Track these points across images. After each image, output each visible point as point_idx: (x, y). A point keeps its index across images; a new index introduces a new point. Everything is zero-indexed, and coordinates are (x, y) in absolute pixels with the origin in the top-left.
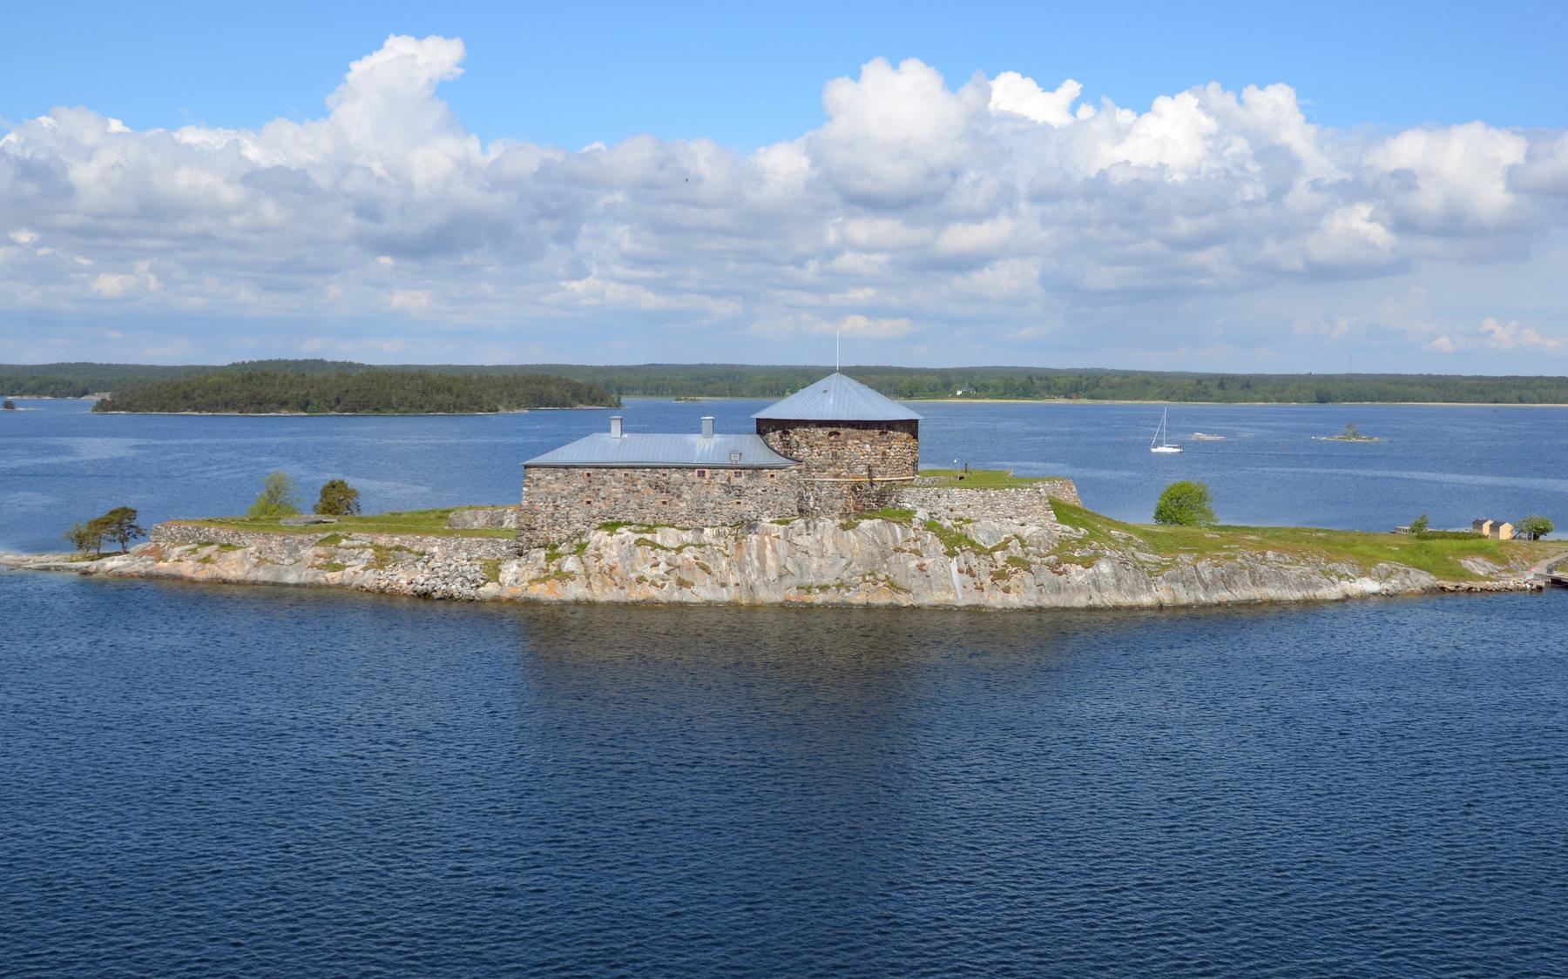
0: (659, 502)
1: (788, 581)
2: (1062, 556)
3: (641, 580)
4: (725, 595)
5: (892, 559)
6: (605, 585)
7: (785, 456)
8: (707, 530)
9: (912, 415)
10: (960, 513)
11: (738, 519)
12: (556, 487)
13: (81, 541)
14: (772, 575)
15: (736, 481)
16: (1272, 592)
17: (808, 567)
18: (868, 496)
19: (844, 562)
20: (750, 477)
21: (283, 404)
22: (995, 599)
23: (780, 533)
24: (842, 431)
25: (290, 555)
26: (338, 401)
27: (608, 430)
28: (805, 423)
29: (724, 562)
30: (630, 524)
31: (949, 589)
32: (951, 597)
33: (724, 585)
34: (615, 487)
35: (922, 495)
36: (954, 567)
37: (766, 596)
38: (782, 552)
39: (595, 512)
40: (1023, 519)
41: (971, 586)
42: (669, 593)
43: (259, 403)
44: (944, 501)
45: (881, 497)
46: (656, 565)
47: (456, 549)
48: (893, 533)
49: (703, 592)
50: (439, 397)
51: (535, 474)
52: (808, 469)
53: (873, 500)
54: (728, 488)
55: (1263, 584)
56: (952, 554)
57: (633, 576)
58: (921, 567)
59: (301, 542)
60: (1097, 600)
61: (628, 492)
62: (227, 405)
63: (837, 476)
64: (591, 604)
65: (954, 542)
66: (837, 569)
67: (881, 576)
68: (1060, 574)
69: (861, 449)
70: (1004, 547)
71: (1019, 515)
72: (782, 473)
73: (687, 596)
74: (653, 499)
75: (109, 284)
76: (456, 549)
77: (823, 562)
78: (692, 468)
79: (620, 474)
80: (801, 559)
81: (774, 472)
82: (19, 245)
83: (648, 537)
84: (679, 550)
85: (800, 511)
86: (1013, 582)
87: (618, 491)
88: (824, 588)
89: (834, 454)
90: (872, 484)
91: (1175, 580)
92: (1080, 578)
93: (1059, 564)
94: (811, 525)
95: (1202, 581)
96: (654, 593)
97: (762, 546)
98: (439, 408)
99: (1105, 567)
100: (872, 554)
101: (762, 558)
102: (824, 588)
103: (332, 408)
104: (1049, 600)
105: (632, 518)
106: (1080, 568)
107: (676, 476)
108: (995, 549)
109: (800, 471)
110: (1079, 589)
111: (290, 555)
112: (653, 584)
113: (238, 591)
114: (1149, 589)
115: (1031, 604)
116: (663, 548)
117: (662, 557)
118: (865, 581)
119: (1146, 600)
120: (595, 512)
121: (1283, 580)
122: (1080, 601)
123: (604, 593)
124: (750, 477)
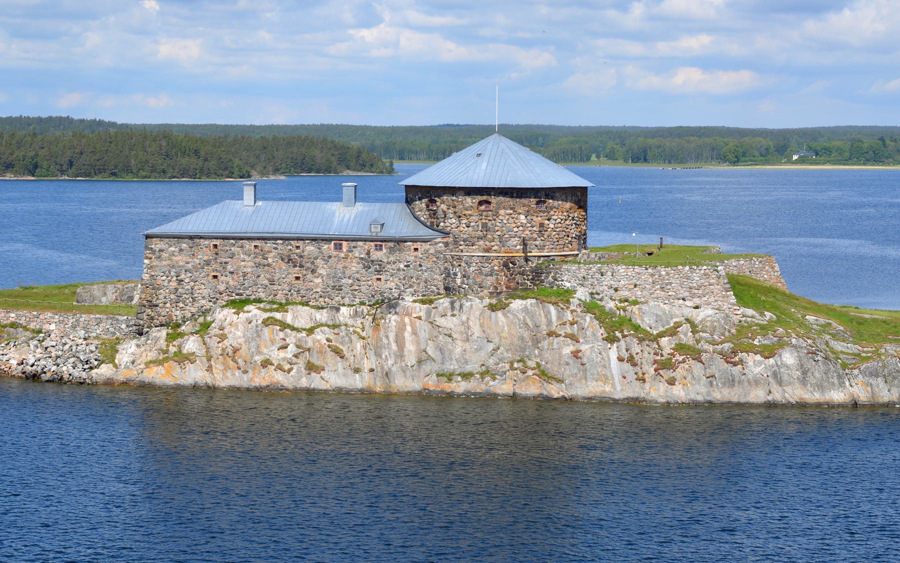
0: (291, 278)
1: (427, 367)
3: (266, 363)
4: (358, 382)
5: (545, 344)
6: (227, 368)
7: (431, 227)
10: (624, 293)
11: (378, 297)
12: (180, 259)
14: (411, 360)
15: (376, 255)
17: (451, 352)
19: (491, 347)
20: (391, 251)
22: (657, 392)
23: (422, 314)
24: (494, 200)
26: (71, 164)
28: (452, 191)
29: (359, 345)
30: (259, 301)
31: (606, 379)
32: (608, 388)
33: (357, 371)
34: (243, 260)
35: (583, 272)
36: (613, 354)
37: (403, 383)
38: (423, 335)
41: (631, 376)
44: (607, 280)
45: (537, 273)
47: (74, 327)
48: (548, 314)
49: (334, 377)
50: (184, 161)
51: (157, 245)
52: (456, 242)
53: (527, 278)
54: (368, 263)
57: (258, 359)
58: (576, 354)
61: (258, 265)
63: (488, 250)
64: (211, 389)
65: (615, 326)
66: (483, 353)
67: (531, 364)
69: (515, 221)
70: (672, 332)
71: (693, 296)
72: (426, 246)
73: (316, 382)
74: (285, 273)
76: (74, 327)
77: (467, 346)
78: (328, 240)
79: (249, 246)
80: (448, 342)
81: (416, 245)
83: (278, 316)
84: (310, 331)
86: (679, 372)
87: (248, 265)
88: (466, 376)
89: (485, 226)
90: (527, 259)
91: (875, 374)
92: (757, 370)
93: (734, 353)
94: (457, 305)
96: (280, 378)
97: (401, 328)
99: (788, 358)
100: (522, 338)
102: (466, 376)
103: (63, 172)
104: (720, 394)
105: (262, 295)
106: (758, 357)
107: (310, 248)
109: (446, 244)
110: (757, 382)
112: (280, 368)
114: (842, 384)
115: (700, 398)
116: (293, 329)
117: (292, 338)
118: (512, 368)
119: (837, 396)
120: (222, 287)
122: (758, 395)
123: (225, 377)
124: (391, 251)
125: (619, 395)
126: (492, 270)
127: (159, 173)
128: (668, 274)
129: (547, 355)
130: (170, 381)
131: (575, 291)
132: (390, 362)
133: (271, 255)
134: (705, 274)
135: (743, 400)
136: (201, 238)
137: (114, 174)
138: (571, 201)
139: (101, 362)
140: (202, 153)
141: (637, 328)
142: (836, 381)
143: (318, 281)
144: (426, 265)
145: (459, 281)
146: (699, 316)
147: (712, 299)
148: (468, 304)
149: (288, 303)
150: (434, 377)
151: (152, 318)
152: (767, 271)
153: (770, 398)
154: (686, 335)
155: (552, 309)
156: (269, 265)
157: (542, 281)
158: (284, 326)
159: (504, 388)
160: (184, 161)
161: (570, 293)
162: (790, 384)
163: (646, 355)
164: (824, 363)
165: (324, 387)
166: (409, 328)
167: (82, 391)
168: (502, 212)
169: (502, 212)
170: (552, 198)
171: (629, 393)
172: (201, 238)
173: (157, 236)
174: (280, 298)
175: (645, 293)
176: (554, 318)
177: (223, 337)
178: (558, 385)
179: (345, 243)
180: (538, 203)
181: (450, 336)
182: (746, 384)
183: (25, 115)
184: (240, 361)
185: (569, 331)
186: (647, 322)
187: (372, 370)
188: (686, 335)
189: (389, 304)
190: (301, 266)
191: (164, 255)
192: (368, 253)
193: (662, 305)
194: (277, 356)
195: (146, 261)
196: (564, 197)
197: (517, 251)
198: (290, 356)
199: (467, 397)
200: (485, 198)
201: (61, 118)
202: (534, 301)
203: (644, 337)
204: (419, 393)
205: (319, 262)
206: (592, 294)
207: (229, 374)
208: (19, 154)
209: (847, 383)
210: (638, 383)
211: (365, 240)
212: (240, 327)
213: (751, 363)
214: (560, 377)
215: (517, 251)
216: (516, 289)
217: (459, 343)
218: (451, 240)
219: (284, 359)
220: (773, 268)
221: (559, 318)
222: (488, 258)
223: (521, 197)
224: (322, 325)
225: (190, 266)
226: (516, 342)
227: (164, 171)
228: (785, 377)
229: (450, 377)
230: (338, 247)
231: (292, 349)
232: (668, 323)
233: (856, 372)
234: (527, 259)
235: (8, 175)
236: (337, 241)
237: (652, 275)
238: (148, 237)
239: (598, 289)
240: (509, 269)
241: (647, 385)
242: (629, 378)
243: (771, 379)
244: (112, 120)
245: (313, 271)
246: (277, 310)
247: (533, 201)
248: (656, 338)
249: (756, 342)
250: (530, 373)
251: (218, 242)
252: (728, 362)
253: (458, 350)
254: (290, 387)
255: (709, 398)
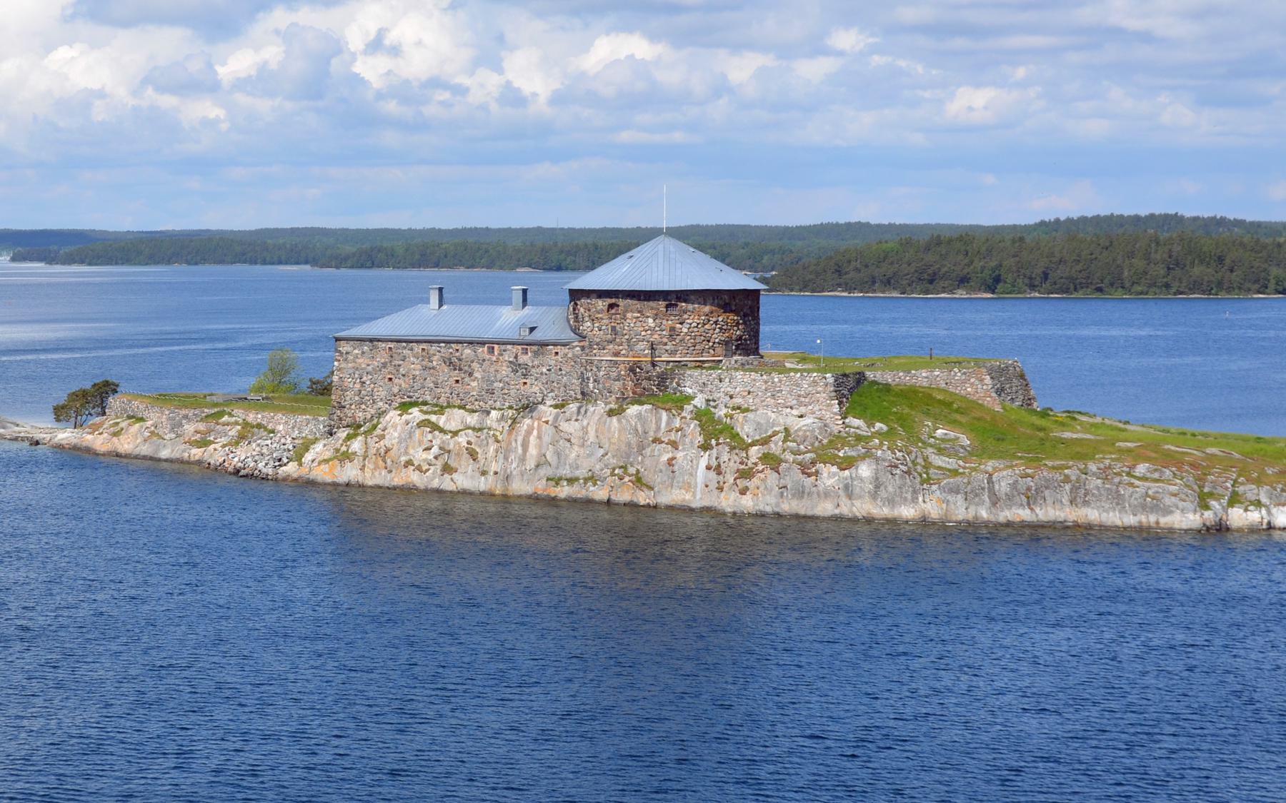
1: (544, 472)
2: (828, 451)
3: (409, 463)
4: (482, 484)
5: (648, 451)
8: (494, 413)
9: (751, 284)
10: (738, 401)
11: (525, 402)
12: (362, 361)
13: (60, 413)
14: (531, 464)
15: (524, 359)
16: (1092, 514)
17: (567, 456)
18: (649, 379)
19: (602, 451)
20: (536, 354)
21: (963, 281)
22: (729, 502)
23: (551, 419)
24: (621, 302)
25: (172, 430)
26: (1045, 276)
27: (427, 301)
29: (492, 448)
30: (425, 403)
32: (688, 497)
33: (484, 473)
35: (704, 379)
36: (703, 463)
37: (520, 487)
38: (547, 439)
39: (396, 390)
40: (803, 410)
41: (713, 485)
42: (434, 480)
43: (929, 280)
44: (725, 387)
45: (663, 379)
46: (429, 449)
48: (659, 420)
49: (465, 479)
50: (1197, 271)
51: (345, 347)
52: (591, 347)
53: (653, 384)
54: (516, 366)
55: (1086, 503)
56: (705, 447)
57: (403, 459)
58: (670, 462)
59: (186, 417)
60: (845, 509)
62: (888, 283)
63: (617, 354)
64: (361, 487)
65: (714, 430)
66: (593, 459)
67: (632, 470)
68: (809, 475)
69: (644, 325)
70: (765, 442)
71: (800, 404)
73: (447, 484)
74: (445, 374)
75: (973, 102)
78: (483, 343)
79: (418, 348)
80: (568, 447)
81: (558, 349)
82: (841, 54)
83: (433, 418)
84: (455, 433)
85: (583, 393)
88: (571, 481)
89: (614, 328)
90: (654, 364)
91: (955, 490)
92: (830, 482)
93: (813, 463)
94: (583, 410)
95: (992, 493)
96: (415, 478)
97: (529, 432)
98: (1196, 286)
99: (865, 470)
100: (629, 445)
101: (525, 446)
102: (571, 481)
103: (1033, 287)
104: (789, 506)
105: (428, 398)
106: (835, 469)
108: (753, 444)
109: (583, 348)
110: (827, 494)
111: (172, 430)
112: (419, 468)
113: (107, 459)
114: (914, 500)
115: (768, 509)
116: (442, 431)
117: (438, 438)
118: (613, 474)
119: (907, 512)
120: (396, 390)
121: (1118, 500)
122: (825, 508)
123: (374, 477)
124: (536, 354)
125: (696, 504)
126: (619, 375)
127: (1160, 287)
128: (780, 381)
129: (647, 462)
130: (329, 479)
131: (693, 398)
132: (514, 465)
133: (435, 358)
134: (814, 382)
135: (810, 513)
136: (379, 340)
137: (1100, 290)
138: (712, 305)
139: (290, 460)
140: (1228, 261)
141: (735, 436)
142: (909, 496)
143: (474, 384)
144: (566, 369)
145: (591, 385)
146: (797, 425)
147: (817, 408)
148: (592, 409)
149: (449, 406)
150: (544, 481)
151: (341, 419)
152: (972, 384)
153: (837, 512)
154: (776, 444)
155: (664, 415)
156: (433, 368)
157: (667, 387)
158: (435, 427)
159: (600, 493)
160: (1197, 271)
161: (689, 398)
162: (860, 497)
163: (732, 463)
164: (902, 477)
165: (450, 489)
166: (535, 432)
167: (268, 487)
168: (629, 315)
169: (629, 315)
170: (685, 301)
171: (706, 503)
172: (379, 340)
173: (347, 339)
174: (443, 401)
175: (757, 400)
176: (663, 425)
177: (382, 437)
178: (647, 492)
179: (496, 347)
180: (667, 307)
181: (569, 441)
182: (815, 496)
183: (1117, 213)
184: (389, 461)
185: (673, 438)
186: (746, 429)
187: (496, 473)
188: (776, 444)
189: (528, 407)
190: (460, 370)
191: (351, 357)
192: (516, 357)
193: (769, 413)
194: (419, 456)
195: (336, 363)
196: (701, 300)
197: (646, 356)
198: (431, 457)
199: (572, 501)
200: (613, 301)
201: (1167, 216)
202: (650, 407)
203: (739, 445)
204: (529, 497)
205: (475, 365)
206: (708, 401)
207: (377, 473)
208: (978, 264)
209: (921, 499)
210: (716, 492)
211: (513, 344)
212: (399, 428)
213: (825, 475)
214: (651, 484)
215: (646, 356)
216: (641, 395)
217: (576, 448)
218: (586, 344)
219: (425, 460)
220: (982, 380)
221: (668, 424)
222: (616, 362)
223: (649, 300)
224: (469, 428)
225: (370, 368)
226: (623, 448)
227: (1167, 286)
228: (857, 491)
229: (557, 481)
230: (491, 350)
231: (435, 450)
232: (766, 431)
233: (934, 487)
234: (654, 364)
235: (960, 291)
236: (490, 344)
237: (766, 382)
238: (337, 339)
239: (716, 395)
240: (635, 374)
241: (723, 494)
242: (711, 487)
243: (841, 492)
244: (1240, 217)
245: (471, 375)
246: (435, 413)
247: (662, 304)
248: (746, 447)
249: (841, 454)
250: (627, 479)
251: (391, 345)
252: (803, 473)
253: (573, 455)
254: (422, 487)
255: (777, 510)
